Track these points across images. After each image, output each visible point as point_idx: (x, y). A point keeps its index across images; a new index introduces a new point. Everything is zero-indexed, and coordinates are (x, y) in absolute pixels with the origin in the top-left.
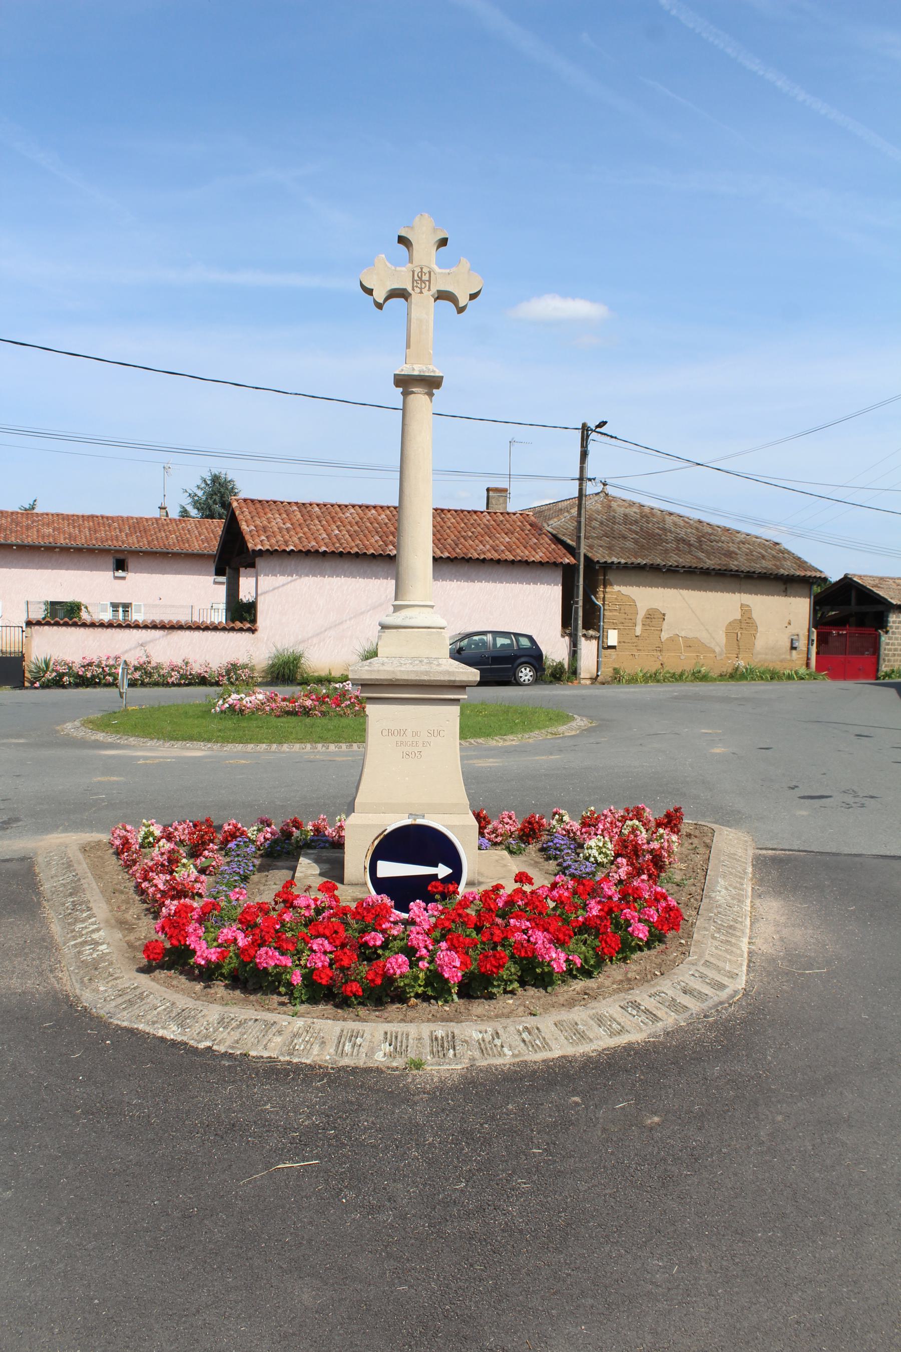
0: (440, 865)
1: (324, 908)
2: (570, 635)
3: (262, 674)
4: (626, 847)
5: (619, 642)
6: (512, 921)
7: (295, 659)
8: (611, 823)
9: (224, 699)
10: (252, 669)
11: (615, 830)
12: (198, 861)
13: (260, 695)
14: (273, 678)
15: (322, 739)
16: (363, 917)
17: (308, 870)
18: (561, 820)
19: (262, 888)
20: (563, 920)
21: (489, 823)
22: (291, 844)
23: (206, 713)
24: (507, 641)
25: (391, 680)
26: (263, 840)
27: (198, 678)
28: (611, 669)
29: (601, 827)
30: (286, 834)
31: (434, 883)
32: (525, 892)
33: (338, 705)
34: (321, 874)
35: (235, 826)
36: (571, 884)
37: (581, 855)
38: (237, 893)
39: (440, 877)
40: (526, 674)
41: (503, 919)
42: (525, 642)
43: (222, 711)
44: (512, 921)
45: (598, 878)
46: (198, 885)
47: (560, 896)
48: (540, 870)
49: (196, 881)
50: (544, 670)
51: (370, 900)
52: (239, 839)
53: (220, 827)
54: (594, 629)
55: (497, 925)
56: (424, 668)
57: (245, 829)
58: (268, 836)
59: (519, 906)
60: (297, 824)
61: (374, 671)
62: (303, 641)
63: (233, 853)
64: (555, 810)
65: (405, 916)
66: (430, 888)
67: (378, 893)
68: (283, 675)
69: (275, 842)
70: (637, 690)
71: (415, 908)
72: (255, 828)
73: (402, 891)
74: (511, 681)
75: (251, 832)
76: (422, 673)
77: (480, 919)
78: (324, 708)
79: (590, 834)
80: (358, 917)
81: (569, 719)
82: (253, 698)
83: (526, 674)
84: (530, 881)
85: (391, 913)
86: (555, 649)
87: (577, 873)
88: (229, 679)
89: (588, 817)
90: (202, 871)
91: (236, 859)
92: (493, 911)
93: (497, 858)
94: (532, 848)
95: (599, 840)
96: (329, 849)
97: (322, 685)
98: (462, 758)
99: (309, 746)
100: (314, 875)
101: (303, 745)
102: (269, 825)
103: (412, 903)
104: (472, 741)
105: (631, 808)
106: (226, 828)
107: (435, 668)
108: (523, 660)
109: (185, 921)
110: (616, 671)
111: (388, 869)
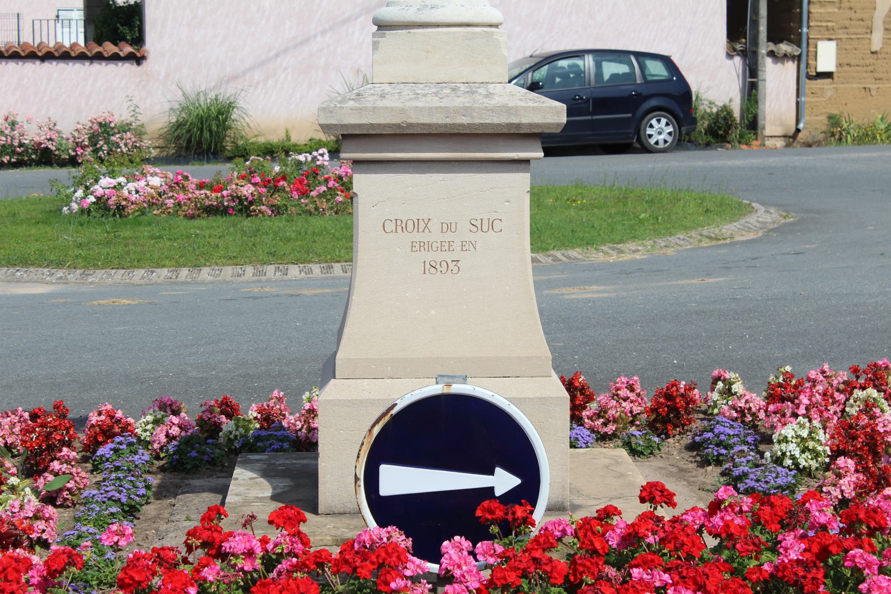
0: (498, 470)
1: (280, 555)
2: (743, 54)
3: (160, 142)
4: (854, 438)
5: (839, 65)
6: (635, 572)
7: (220, 113)
8: (825, 394)
9: (87, 188)
10: (140, 133)
11: (833, 409)
12: (41, 481)
13: (156, 179)
14: (180, 148)
15: (274, 257)
16: (355, 569)
17: (249, 490)
18: (728, 392)
19: (163, 527)
20: (733, 572)
21: (590, 398)
22: (217, 446)
23: (52, 214)
24: (622, 69)
25: (398, 126)
26: (163, 440)
27: (35, 151)
28: (824, 118)
29: (805, 401)
30: (209, 428)
31: (486, 504)
32: (660, 519)
33: (304, 194)
34: (274, 498)
35: (111, 415)
36: (746, 502)
37: (768, 454)
38: (115, 533)
39: (498, 493)
40: (660, 130)
41: (619, 569)
42: (657, 70)
43: (82, 211)
44: (635, 572)
45: (799, 496)
46: (40, 525)
47: (727, 525)
48: (690, 484)
49: (36, 517)
50: (694, 121)
51: (366, 538)
52: (118, 439)
53: (84, 420)
54: (790, 41)
55: (609, 580)
56: (460, 101)
57: (131, 420)
58: (175, 431)
59: (649, 545)
60: (229, 409)
61: (365, 109)
62: (235, 77)
63: (107, 465)
64: (716, 373)
65: (434, 568)
66: (479, 513)
67: (382, 523)
68: (199, 143)
69: (187, 442)
70: (874, 155)
71: (452, 552)
72: (150, 418)
73: (427, 522)
74: (631, 143)
75: (142, 426)
76: (457, 111)
77: (575, 570)
78: (277, 200)
79: (784, 415)
80: (346, 569)
81: (741, 210)
82: (142, 183)
83: (660, 130)
84: (669, 499)
85: (407, 561)
86: (715, 81)
87: (761, 487)
88: (95, 151)
89: (780, 385)
90: (50, 499)
91: (113, 475)
92: (599, 555)
93: (607, 461)
94: (674, 446)
95: (802, 426)
96: (290, 452)
97: (273, 159)
98: (538, 285)
99: (249, 270)
100: (261, 499)
101: (238, 269)
102: (176, 413)
103: (446, 543)
104: (558, 254)
105: (863, 367)
106: (94, 419)
107: (481, 101)
108: (653, 102)
109: (15, 587)
110: (834, 120)
111: (398, 480)
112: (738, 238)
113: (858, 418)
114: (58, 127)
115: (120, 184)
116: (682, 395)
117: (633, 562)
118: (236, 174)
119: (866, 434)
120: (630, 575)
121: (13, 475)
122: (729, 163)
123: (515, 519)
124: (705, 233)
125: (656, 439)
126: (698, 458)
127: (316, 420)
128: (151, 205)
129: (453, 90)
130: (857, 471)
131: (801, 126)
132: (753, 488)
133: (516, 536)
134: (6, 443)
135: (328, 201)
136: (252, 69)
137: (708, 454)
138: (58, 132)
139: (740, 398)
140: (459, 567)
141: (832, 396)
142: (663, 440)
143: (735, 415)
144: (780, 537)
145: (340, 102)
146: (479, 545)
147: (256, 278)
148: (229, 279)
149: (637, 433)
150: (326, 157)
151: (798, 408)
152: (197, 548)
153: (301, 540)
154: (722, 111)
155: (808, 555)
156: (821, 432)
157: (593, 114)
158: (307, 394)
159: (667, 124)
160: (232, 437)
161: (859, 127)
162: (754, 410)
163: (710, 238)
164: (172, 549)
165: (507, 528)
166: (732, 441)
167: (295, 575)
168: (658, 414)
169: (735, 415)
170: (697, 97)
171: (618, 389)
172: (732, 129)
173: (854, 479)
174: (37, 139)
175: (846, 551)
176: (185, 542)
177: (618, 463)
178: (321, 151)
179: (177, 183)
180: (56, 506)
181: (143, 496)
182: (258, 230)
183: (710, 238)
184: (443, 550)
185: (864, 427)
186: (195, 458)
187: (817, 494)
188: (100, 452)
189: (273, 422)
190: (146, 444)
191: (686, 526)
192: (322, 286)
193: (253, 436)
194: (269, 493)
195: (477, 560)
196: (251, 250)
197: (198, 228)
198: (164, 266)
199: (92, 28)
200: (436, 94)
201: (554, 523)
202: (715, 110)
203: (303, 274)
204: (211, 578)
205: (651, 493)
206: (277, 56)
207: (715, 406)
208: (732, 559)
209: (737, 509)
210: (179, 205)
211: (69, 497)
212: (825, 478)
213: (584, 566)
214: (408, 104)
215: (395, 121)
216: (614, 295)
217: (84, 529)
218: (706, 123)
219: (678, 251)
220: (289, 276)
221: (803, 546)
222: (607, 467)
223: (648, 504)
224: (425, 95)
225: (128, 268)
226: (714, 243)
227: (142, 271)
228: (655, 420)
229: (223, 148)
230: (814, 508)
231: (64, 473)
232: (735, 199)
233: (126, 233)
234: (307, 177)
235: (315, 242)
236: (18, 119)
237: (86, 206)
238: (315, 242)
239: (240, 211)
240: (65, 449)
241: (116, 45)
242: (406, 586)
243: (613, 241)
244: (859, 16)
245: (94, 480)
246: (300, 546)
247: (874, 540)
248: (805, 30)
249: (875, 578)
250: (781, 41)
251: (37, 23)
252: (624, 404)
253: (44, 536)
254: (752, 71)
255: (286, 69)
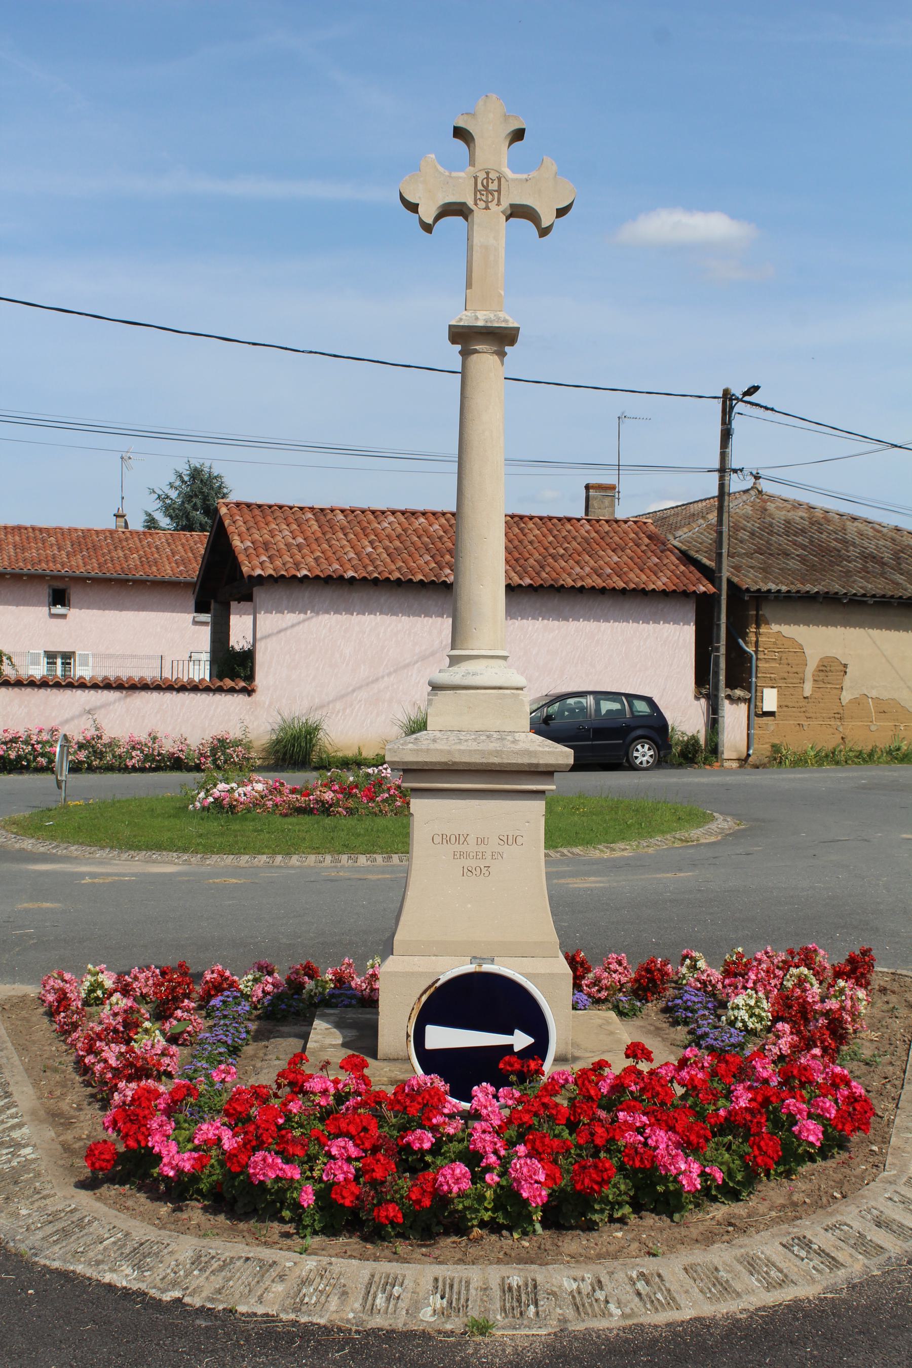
0: (517, 1032)
1: (348, 1093)
2: (707, 697)
4: (790, 1007)
5: (780, 706)
6: (621, 1115)
8: (768, 971)
9: (208, 791)
10: (248, 748)
11: (773, 982)
12: (168, 1025)
14: (277, 759)
15: (348, 849)
16: (405, 1108)
17: (325, 1038)
18: (694, 967)
19: (259, 1064)
20: (697, 1114)
22: (302, 1001)
23: (181, 810)
24: (616, 706)
25: (446, 763)
26: (260, 994)
27: (169, 759)
28: (768, 746)
29: (753, 977)
30: (295, 986)
31: (507, 1058)
32: (640, 1072)
33: (372, 799)
34: (345, 1045)
35: (221, 974)
38: (223, 1072)
39: (516, 1049)
40: (643, 753)
42: (642, 707)
44: (621, 1115)
45: (747, 1053)
46: (166, 1060)
47: (692, 1078)
48: (664, 1040)
49: (163, 1054)
51: (414, 1082)
52: (226, 993)
54: (743, 688)
55: (600, 1120)
56: (493, 746)
58: (269, 988)
59: (632, 1093)
60: (311, 971)
61: (421, 750)
62: (322, 707)
63: (218, 1013)
64: (685, 952)
65: (466, 1106)
66: (501, 1066)
67: (427, 1072)
69: (278, 998)
71: (480, 1095)
72: (250, 977)
73: (462, 1070)
74: (620, 762)
75: (244, 983)
76: (491, 753)
77: (575, 1112)
78: (351, 803)
79: (736, 988)
81: (705, 819)
82: (249, 788)
83: (643, 753)
84: (647, 1055)
85: (446, 1101)
86: (686, 716)
88: (214, 761)
89: (734, 963)
90: (173, 1039)
91: (222, 1022)
93: (600, 1021)
94: (652, 1008)
95: (750, 997)
96: (356, 1008)
97: (349, 770)
98: (549, 876)
99: (328, 858)
100: (334, 1046)
101: (320, 857)
102: (270, 973)
103: (475, 1088)
104: (565, 851)
105: (797, 949)
106: (209, 976)
107: (509, 746)
108: (639, 732)
110: (776, 748)
111: (440, 1037)
112: (703, 841)
113: (793, 991)
114: (188, 742)
115: (232, 788)
116: (659, 970)
117: (620, 1107)
118: (320, 782)
119: (799, 1004)
120: (617, 1117)
121: (147, 1020)
122: (696, 780)
123: (529, 1071)
124: (677, 836)
125: (639, 1004)
126: (671, 1020)
127: (377, 983)
128: (255, 805)
129: (488, 737)
130: (792, 1033)
131: (751, 752)
132: (712, 1045)
133: (530, 1083)
134: (142, 993)
135: (390, 805)
136: (335, 700)
137: (678, 1017)
138: (188, 745)
139: (703, 972)
140: (486, 1107)
141: (773, 972)
142: (643, 1005)
143: (699, 986)
144: (732, 1088)
145: (402, 745)
146: (501, 1090)
147: (333, 864)
148: (312, 864)
149: (624, 999)
150: (389, 771)
151: (747, 982)
152: (285, 1085)
153: (364, 1081)
154: (691, 739)
155: (754, 1104)
156: (765, 1001)
157: (592, 740)
158: (371, 961)
159: (649, 749)
160: (312, 994)
161: (795, 753)
162: (713, 982)
163: (681, 840)
164: (266, 1087)
165: (523, 1077)
166: (696, 1007)
167: (359, 1111)
168: (640, 984)
169: (699, 986)
170: (673, 728)
171: (609, 963)
172: (699, 753)
173: (789, 1039)
174: (171, 750)
175: (783, 1101)
176: (276, 1081)
177: (609, 1023)
178: (385, 766)
179: (275, 789)
180: (178, 1045)
181: (244, 1039)
182: (336, 827)
183: (681, 840)
184: (474, 1093)
185: (798, 998)
186: (284, 1010)
187: (761, 1052)
188: (212, 1003)
189: (344, 983)
190: (247, 997)
191: (661, 1078)
192: (383, 873)
193: (329, 994)
194: (340, 1041)
195: (498, 1101)
196: (330, 842)
197: (290, 824)
198: (263, 854)
199: (216, 667)
200: (475, 740)
201: (559, 1073)
202: (686, 738)
203: (369, 862)
204: (295, 1111)
205: (634, 1051)
206: (354, 691)
207: (684, 977)
208: (695, 1104)
209: (700, 1065)
210: (276, 805)
211: (188, 1038)
212: (767, 1038)
213: (582, 1108)
214: (454, 747)
215: (444, 759)
216: (607, 885)
217: (199, 1064)
218: (680, 748)
219: (656, 850)
220: (358, 864)
221: (750, 1096)
222: (600, 1026)
223: (631, 1060)
224: (466, 741)
225: (236, 854)
226: (685, 844)
227: (247, 857)
228: (638, 989)
229: (310, 761)
230: (757, 1063)
231: (185, 1019)
232: (701, 809)
233: (236, 826)
234: (374, 786)
235: (378, 837)
236: (158, 735)
237: (206, 804)
238: (378, 837)
239: (323, 812)
240: (186, 1001)
241: (233, 681)
242: (444, 1122)
243: (607, 842)
244: (794, 670)
245: (207, 1025)
246: (364, 1086)
247: (804, 1092)
248: (754, 680)
249: (804, 1122)
250: (736, 688)
251: (175, 664)
252: (614, 975)
253: (169, 1069)
254: (714, 711)
255: (360, 701)
